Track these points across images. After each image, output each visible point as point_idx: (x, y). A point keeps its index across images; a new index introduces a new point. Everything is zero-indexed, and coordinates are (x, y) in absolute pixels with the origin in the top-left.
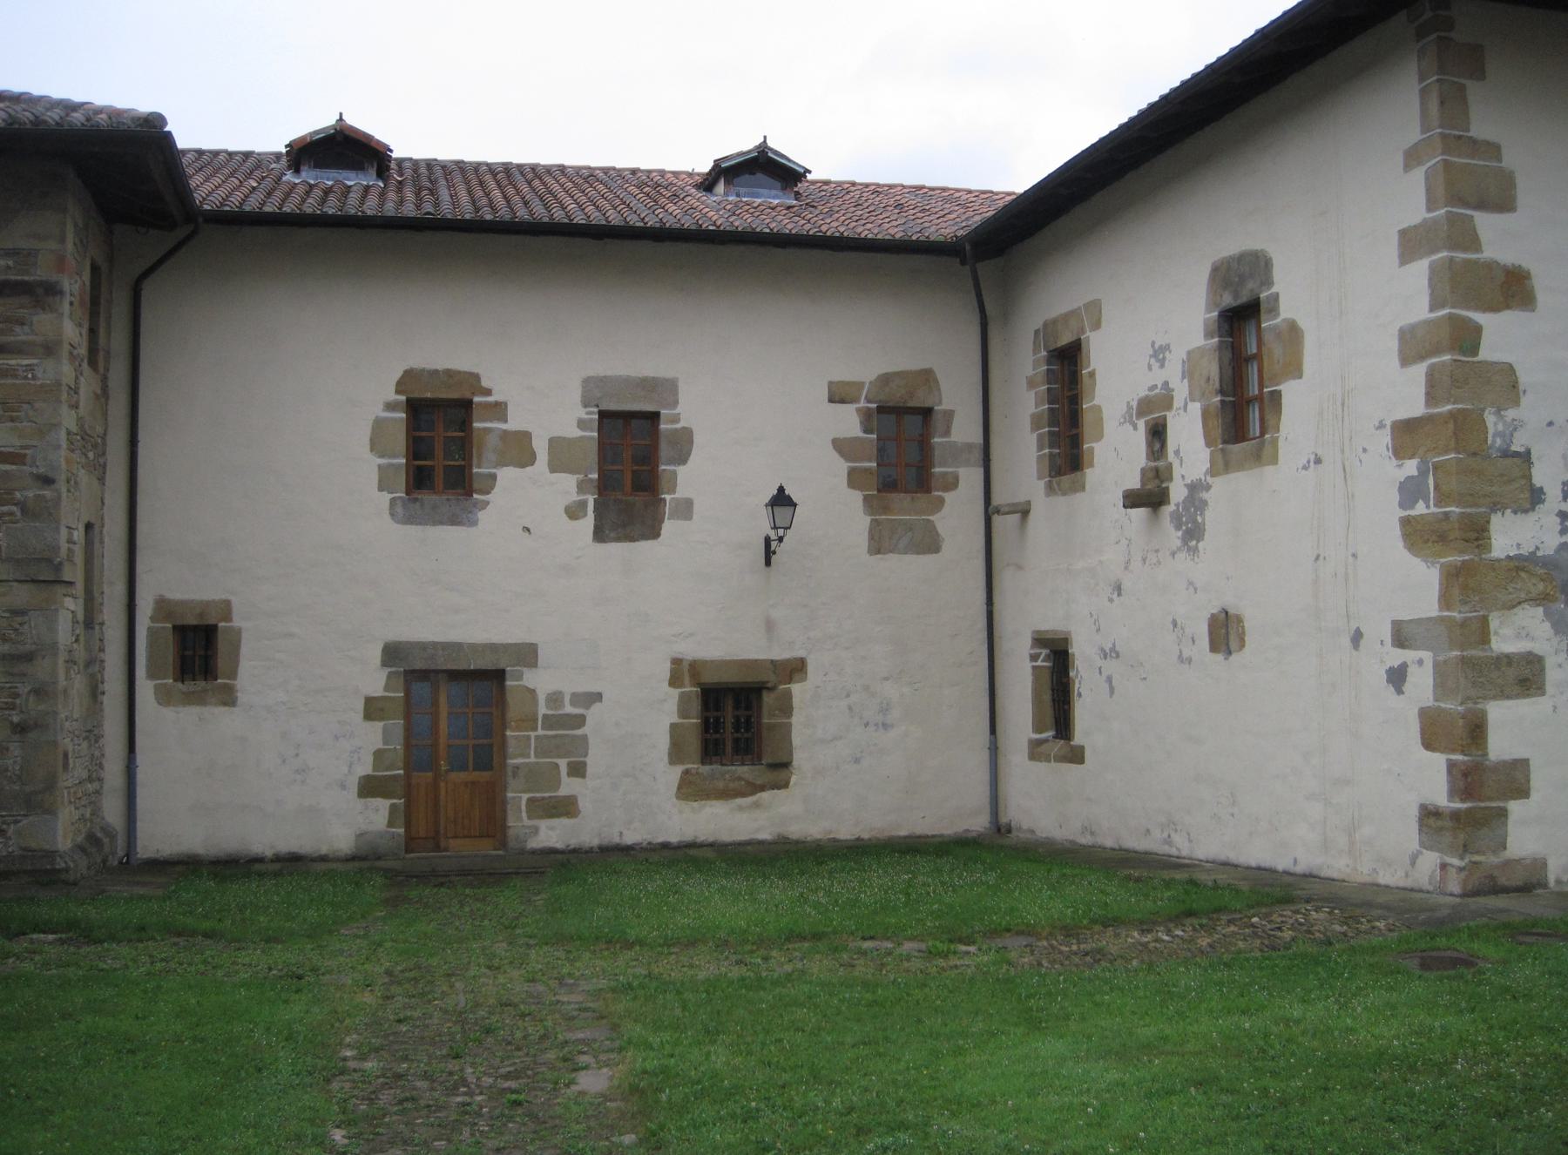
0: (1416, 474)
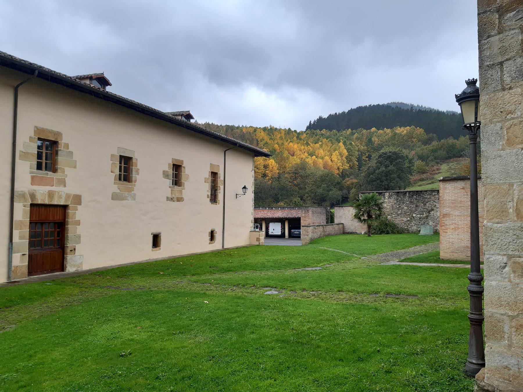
0: (298, 132)
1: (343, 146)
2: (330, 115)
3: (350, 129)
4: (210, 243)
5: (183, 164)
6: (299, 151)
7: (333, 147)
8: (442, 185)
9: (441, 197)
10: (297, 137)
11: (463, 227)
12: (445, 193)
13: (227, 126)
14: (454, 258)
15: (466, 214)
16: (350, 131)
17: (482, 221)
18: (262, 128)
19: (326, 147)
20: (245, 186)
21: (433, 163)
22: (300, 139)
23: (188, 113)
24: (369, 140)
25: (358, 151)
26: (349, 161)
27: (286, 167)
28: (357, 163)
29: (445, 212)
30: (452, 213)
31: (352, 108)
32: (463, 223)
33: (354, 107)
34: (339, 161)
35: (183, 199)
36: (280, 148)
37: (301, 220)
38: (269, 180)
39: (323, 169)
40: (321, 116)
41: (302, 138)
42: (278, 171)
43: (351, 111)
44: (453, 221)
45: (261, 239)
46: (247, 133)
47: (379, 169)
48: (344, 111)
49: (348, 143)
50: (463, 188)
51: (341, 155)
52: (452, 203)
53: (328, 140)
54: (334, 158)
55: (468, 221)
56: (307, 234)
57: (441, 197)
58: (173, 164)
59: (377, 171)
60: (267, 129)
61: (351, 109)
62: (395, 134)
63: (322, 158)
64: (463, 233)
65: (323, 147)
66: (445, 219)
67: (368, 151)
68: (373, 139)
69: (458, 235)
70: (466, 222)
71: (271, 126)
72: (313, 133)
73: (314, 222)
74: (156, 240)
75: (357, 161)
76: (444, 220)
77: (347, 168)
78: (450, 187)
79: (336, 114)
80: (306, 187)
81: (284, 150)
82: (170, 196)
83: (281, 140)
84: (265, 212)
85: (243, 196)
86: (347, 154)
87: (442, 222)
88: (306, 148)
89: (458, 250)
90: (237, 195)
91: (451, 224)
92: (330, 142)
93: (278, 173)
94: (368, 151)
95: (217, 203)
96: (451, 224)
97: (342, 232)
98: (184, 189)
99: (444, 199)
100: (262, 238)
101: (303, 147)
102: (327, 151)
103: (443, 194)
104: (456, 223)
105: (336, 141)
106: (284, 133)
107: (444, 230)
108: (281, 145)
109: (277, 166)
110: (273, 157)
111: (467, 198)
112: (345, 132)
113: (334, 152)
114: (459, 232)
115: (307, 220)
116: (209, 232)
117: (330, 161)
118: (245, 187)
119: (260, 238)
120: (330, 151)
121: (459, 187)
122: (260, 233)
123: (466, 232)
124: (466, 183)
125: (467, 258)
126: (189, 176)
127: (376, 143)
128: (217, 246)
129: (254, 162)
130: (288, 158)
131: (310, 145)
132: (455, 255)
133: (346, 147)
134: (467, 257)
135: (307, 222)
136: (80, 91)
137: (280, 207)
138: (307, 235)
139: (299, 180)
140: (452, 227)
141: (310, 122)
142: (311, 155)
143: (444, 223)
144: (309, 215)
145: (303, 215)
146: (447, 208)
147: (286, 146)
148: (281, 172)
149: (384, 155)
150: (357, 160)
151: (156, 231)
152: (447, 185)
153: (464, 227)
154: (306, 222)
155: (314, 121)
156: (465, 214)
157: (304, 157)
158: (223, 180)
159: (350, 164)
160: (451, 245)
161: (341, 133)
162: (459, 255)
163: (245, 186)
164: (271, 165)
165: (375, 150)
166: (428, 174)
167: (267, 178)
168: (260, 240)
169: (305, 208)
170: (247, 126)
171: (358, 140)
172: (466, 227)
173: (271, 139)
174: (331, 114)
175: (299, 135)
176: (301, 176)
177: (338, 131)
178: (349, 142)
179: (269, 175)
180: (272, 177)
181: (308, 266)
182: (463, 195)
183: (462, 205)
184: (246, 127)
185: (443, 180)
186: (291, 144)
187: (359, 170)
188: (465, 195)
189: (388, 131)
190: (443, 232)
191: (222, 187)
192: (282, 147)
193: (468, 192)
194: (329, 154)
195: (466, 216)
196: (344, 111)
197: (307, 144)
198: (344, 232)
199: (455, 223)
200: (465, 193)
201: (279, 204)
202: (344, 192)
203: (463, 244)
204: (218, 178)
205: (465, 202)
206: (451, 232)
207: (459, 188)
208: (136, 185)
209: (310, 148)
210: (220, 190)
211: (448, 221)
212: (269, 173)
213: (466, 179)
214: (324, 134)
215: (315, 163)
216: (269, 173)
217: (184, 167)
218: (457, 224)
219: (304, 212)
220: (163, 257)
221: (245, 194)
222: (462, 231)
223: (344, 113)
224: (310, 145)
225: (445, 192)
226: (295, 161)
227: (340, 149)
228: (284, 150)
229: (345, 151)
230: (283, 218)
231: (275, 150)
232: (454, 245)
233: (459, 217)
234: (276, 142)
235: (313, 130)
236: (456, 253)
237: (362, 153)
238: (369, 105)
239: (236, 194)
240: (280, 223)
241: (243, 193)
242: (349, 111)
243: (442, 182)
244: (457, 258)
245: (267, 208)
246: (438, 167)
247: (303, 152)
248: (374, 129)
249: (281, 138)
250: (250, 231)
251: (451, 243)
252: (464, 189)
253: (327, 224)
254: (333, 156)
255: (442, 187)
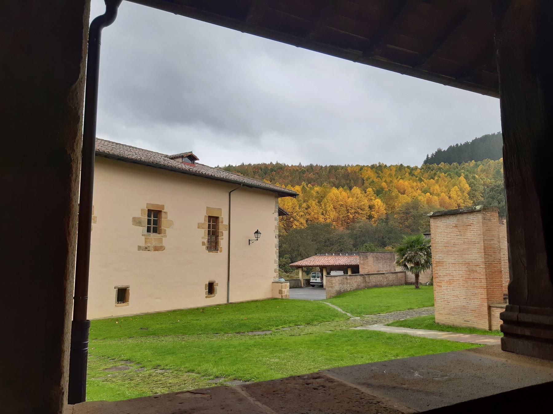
1: (465, 180)
2: (451, 147)
3: (473, 161)
4: (206, 297)
5: (163, 209)
6: (410, 188)
7: (452, 181)
8: (433, 222)
9: (433, 239)
10: (410, 173)
11: (458, 279)
12: (437, 233)
13: (332, 167)
14: (451, 322)
15: (461, 262)
16: (474, 162)
17: (479, 271)
18: (370, 166)
19: (443, 182)
20: (258, 230)
22: (413, 175)
23: (190, 154)
24: (497, 171)
25: (484, 185)
26: (473, 197)
27: (395, 207)
29: (437, 259)
30: (445, 260)
31: (477, 138)
32: (458, 274)
33: (479, 136)
34: (459, 198)
35: (164, 248)
36: (388, 186)
37: (360, 268)
38: (375, 222)
39: (439, 207)
40: (439, 148)
41: (416, 173)
42: (385, 212)
44: (448, 271)
45: (285, 291)
46: (352, 172)
48: (467, 142)
49: (470, 176)
50: (456, 227)
51: (462, 190)
52: (445, 247)
53: (447, 174)
54: (453, 194)
55: (464, 272)
56: (332, 285)
57: (433, 239)
58: (148, 210)
60: (376, 167)
61: (476, 138)
63: (438, 195)
64: (459, 287)
65: (439, 183)
66: (438, 268)
69: (453, 290)
70: (461, 273)
71: (380, 163)
72: (429, 167)
74: (211, 288)
76: (437, 270)
77: (470, 205)
78: (442, 226)
79: (457, 145)
80: (419, 228)
81: (393, 188)
82: (143, 244)
83: (390, 178)
84: (330, 258)
85: (255, 242)
86: (469, 189)
87: (435, 272)
88: (419, 184)
89: (454, 312)
90: (250, 241)
91: (445, 276)
92: (449, 177)
93: (386, 214)
95: (219, 251)
96: (445, 276)
97: (403, 282)
98: (165, 236)
99: (436, 241)
100: (285, 290)
101: (415, 184)
102: (444, 187)
103: (434, 235)
104: (450, 274)
105: (455, 175)
106: (394, 170)
107: (438, 283)
108: (389, 183)
109: (384, 206)
110: (379, 197)
111: (461, 239)
112: (467, 164)
113: (453, 187)
114: (454, 287)
115: (366, 267)
116: (206, 285)
117: (447, 197)
118: (257, 232)
119: (282, 291)
120: (448, 186)
121: (451, 224)
122: (283, 284)
123: (462, 287)
124: (459, 220)
125: (465, 322)
126: (173, 222)
128: (219, 298)
129: (277, 202)
130: (397, 197)
131: (423, 181)
132: (452, 318)
133: (469, 180)
134: (465, 321)
135: (367, 270)
137: (347, 253)
138: (332, 287)
139: (410, 221)
140: (446, 279)
141: (428, 156)
142: (425, 192)
143: (438, 274)
144: (368, 261)
145: (362, 262)
146: (440, 253)
147: (395, 183)
148: (390, 212)
149: (497, 188)
150: (482, 195)
151: (122, 285)
152: (439, 222)
153: (459, 279)
154: (365, 270)
155: (432, 154)
156: (460, 261)
157: (417, 195)
158: (228, 225)
159: (473, 201)
160: (446, 304)
162: (456, 319)
163: (258, 230)
164: (377, 205)
167: (373, 220)
168: (282, 292)
169: (363, 253)
170: (353, 165)
172: (462, 280)
173: (378, 177)
174: (451, 146)
175: (411, 171)
176: (414, 217)
177: (460, 163)
178: (472, 175)
179: (375, 216)
180: (378, 219)
181: (260, 329)
182: (456, 235)
183: (456, 249)
184: (352, 166)
185: (434, 216)
186: (401, 181)
188: (458, 235)
190: (437, 286)
191: (226, 233)
192: (391, 185)
193: (461, 231)
194: (446, 190)
195: (460, 264)
196: (467, 142)
197: (421, 180)
198: (407, 282)
199: (449, 274)
200: (458, 233)
201: (386, 248)
203: (459, 303)
204: (219, 223)
205: (458, 244)
206: (446, 285)
207: (451, 226)
208: (142, 232)
209: (424, 184)
210: (223, 236)
211: (441, 271)
212: (375, 214)
213: (458, 214)
214: (442, 168)
215: (429, 202)
216: (375, 214)
217: (166, 213)
218: (451, 276)
219: (362, 258)
220: (132, 313)
221: (257, 240)
222: (457, 285)
224: (423, 181)
225: (437, 232)
226: (404, 200)
227: (460, 184)
228: (393, 188)
229: (467, 186)
230: (343, 265)
231: (382, 189)
232: (449, 303)
233: (454, 266)
234: (384, 180)
235: (428, 164)
236: (453, 315)
238: (498, 133)
239: (249, 240)
240: (343, 272)
241: (256, 239)
243: (433, 219)
244: (454, 323)
245: (334, 254)
247: (415, 189)
249: (390, 175)
250: (273, 282)
251: (446, 301)
252: (457, 227)
253: (352, 274)
254: (451, 192)
255: (433, 225)
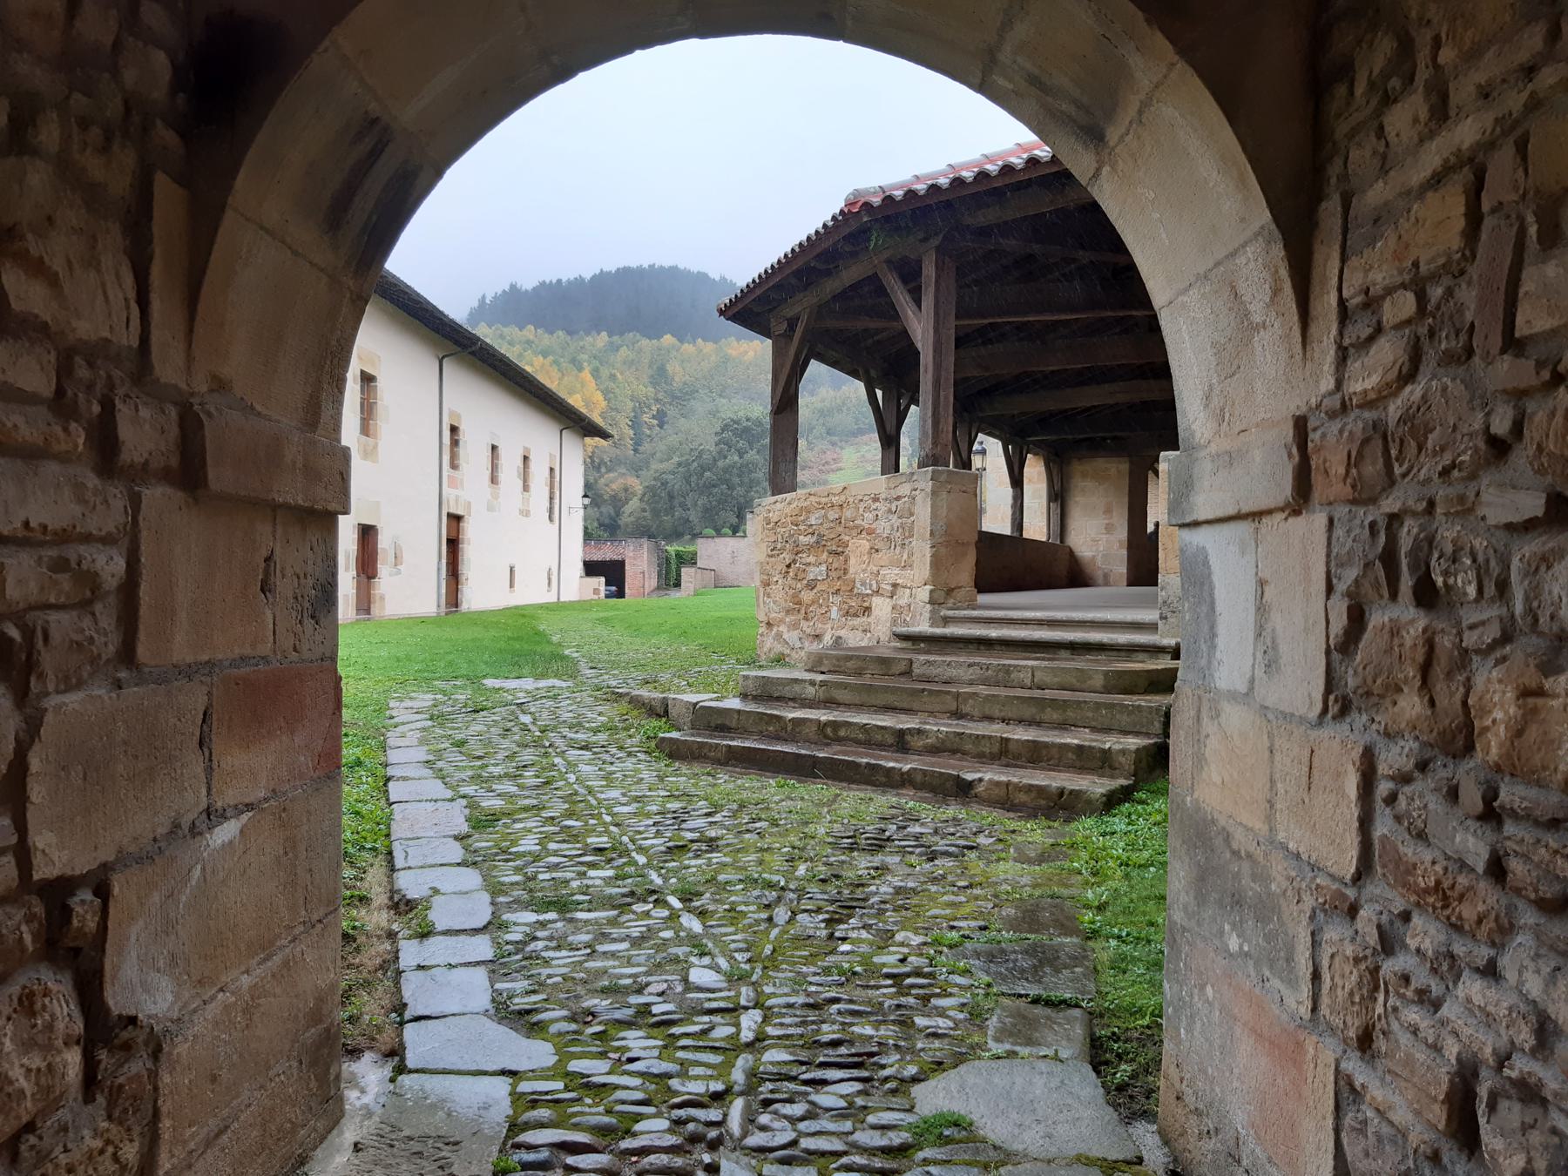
2: (543, 284)
3: (604, 334)
16: (607, 338)
21: (824, 445)
28: (631, 432)
43: (601, 279)
47: (725, 457)
49: (605, 372)
59: (720, 464)
62: (726, 360)
67: (657, 400)
68: (669, 368)
73: (899, 581)
75: (632, 427)
79: (559, 281)
94: (657, 400)
112: (590, 339)
127: (677, 379)
136: (504, 374)
141: (484, 297)
161: (581, 344)
165: (674, 397)
166: (815, 471)
171: (630, 368)
187: (636, 450)
189: (709, 347)
202: (604, 509)
223: (579, 281)
229: (599, 396)
237: (641, 406)
242: (594, 277)
246: (835, 456)
248: (668, 339)
